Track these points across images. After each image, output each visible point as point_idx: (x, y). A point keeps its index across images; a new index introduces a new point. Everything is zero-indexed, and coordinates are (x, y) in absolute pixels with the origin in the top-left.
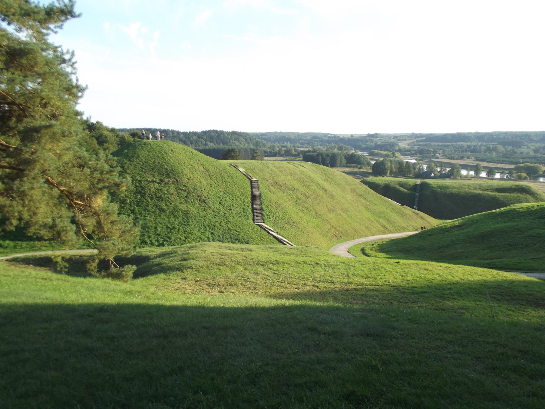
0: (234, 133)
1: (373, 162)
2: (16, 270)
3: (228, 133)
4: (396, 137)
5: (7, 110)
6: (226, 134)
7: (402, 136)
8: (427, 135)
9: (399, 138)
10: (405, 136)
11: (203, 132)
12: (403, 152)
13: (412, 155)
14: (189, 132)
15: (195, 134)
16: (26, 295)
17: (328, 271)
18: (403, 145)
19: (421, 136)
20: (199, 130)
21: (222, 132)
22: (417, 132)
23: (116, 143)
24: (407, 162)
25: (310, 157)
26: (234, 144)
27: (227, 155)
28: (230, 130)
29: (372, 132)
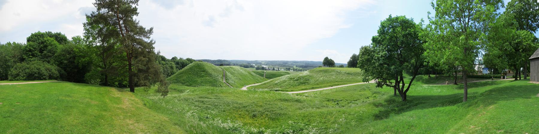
1: (256, 67)
9: (262, 61)
12: (263, 64)
13: (266, 65)
17: (320, 122)
18: (263, 63)
20: (216, 59)
26: (223, 63)
27: (221, 65)
28: (223, 59)
29: (256, 60)
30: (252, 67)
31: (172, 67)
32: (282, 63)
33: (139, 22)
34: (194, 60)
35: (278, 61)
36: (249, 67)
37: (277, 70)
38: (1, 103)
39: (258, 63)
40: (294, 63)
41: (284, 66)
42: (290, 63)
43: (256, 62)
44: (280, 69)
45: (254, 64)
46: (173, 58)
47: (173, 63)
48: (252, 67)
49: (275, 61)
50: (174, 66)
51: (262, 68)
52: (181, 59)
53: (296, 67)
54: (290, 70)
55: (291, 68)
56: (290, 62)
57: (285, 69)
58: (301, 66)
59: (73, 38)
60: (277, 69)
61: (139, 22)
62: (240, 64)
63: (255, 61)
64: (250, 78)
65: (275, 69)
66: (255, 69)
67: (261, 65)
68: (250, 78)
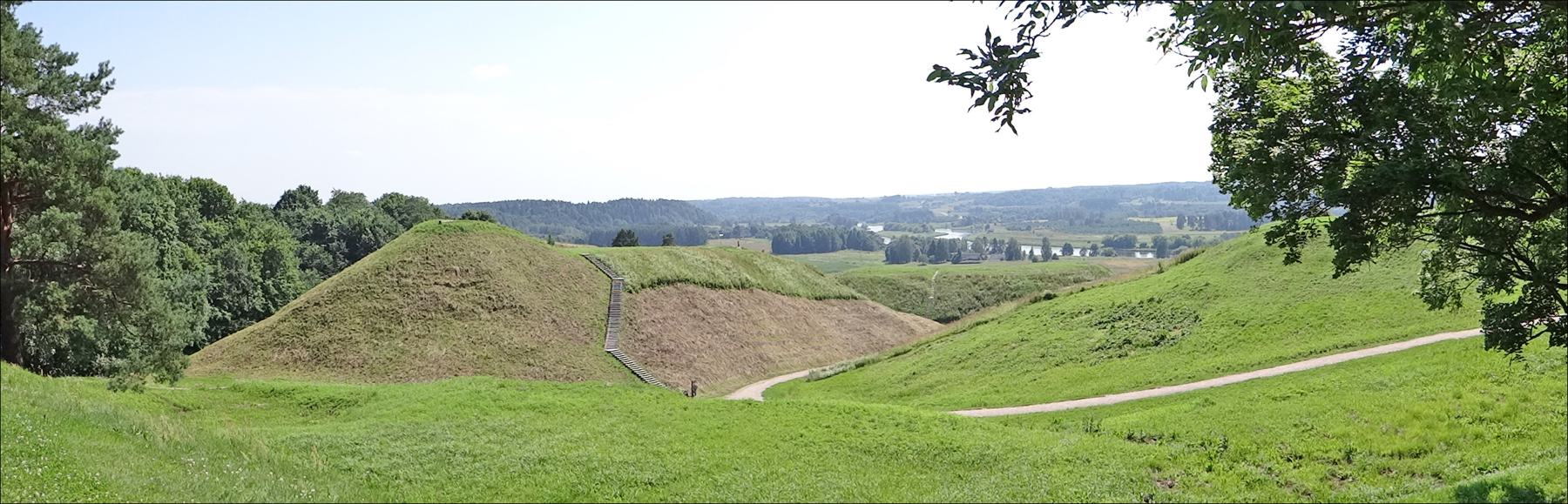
0: (662, 202)
1: (887, 241)
2: (72, 153)
3: (651, 203)
4: (928, 199)
5: (1353, 99)
6: (647, 205)
7: (939, 197)
8: (978, 194)
9: (940, 200)
10: (943, 197)
11: (610, 202)
13: (967, 223)
14: (586, 203)
15: (595, 204)
16: (65, 154)
18: (941, 212)
19: (966, 196)
20: (577, 197)
21: (641, 202)
22: (962, 190)
23: (1378, 465)
24: (940, 240)
25: (467, 216)
29: (890, 194)
30: (860, 242)
31: (271, 261)
32: (1073, 205)
33: (41, 32)
34: (437, 211)
35: (1050, 190)
36: (839, 242)
37: (1035, 260)
38: (1563, 280)
39: (904, 216)
40: (1162, 201)
41: (1092, 224)
42: (1137, 203)
43: (890, 209)
44: (1057, 251)
45: (874, 223)
46: (288, 199)
47: (280, 229)
48: (860, 242)
49: (1024, 192)
50: (287, 245)
51: (930, 253)
52: (340, 199)
53: (1180, 226)
54: (1131, 254)
55: (1142, 238)
56: (1139, 190)
57: (1094, 248)
58: (1217, 218)
59: (28, 27)
60: (1038, 252)
61: (41, 32)
62: (772, 225)
63: (886, 199)
64: (1508, 212)
65: (1026, 249)
66: (881, 255)
67: (925, 230)
68: (1508, 212)
